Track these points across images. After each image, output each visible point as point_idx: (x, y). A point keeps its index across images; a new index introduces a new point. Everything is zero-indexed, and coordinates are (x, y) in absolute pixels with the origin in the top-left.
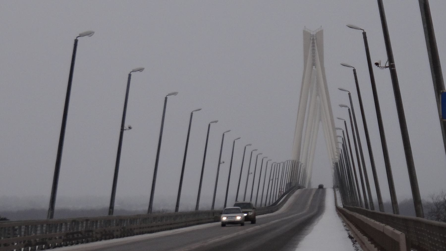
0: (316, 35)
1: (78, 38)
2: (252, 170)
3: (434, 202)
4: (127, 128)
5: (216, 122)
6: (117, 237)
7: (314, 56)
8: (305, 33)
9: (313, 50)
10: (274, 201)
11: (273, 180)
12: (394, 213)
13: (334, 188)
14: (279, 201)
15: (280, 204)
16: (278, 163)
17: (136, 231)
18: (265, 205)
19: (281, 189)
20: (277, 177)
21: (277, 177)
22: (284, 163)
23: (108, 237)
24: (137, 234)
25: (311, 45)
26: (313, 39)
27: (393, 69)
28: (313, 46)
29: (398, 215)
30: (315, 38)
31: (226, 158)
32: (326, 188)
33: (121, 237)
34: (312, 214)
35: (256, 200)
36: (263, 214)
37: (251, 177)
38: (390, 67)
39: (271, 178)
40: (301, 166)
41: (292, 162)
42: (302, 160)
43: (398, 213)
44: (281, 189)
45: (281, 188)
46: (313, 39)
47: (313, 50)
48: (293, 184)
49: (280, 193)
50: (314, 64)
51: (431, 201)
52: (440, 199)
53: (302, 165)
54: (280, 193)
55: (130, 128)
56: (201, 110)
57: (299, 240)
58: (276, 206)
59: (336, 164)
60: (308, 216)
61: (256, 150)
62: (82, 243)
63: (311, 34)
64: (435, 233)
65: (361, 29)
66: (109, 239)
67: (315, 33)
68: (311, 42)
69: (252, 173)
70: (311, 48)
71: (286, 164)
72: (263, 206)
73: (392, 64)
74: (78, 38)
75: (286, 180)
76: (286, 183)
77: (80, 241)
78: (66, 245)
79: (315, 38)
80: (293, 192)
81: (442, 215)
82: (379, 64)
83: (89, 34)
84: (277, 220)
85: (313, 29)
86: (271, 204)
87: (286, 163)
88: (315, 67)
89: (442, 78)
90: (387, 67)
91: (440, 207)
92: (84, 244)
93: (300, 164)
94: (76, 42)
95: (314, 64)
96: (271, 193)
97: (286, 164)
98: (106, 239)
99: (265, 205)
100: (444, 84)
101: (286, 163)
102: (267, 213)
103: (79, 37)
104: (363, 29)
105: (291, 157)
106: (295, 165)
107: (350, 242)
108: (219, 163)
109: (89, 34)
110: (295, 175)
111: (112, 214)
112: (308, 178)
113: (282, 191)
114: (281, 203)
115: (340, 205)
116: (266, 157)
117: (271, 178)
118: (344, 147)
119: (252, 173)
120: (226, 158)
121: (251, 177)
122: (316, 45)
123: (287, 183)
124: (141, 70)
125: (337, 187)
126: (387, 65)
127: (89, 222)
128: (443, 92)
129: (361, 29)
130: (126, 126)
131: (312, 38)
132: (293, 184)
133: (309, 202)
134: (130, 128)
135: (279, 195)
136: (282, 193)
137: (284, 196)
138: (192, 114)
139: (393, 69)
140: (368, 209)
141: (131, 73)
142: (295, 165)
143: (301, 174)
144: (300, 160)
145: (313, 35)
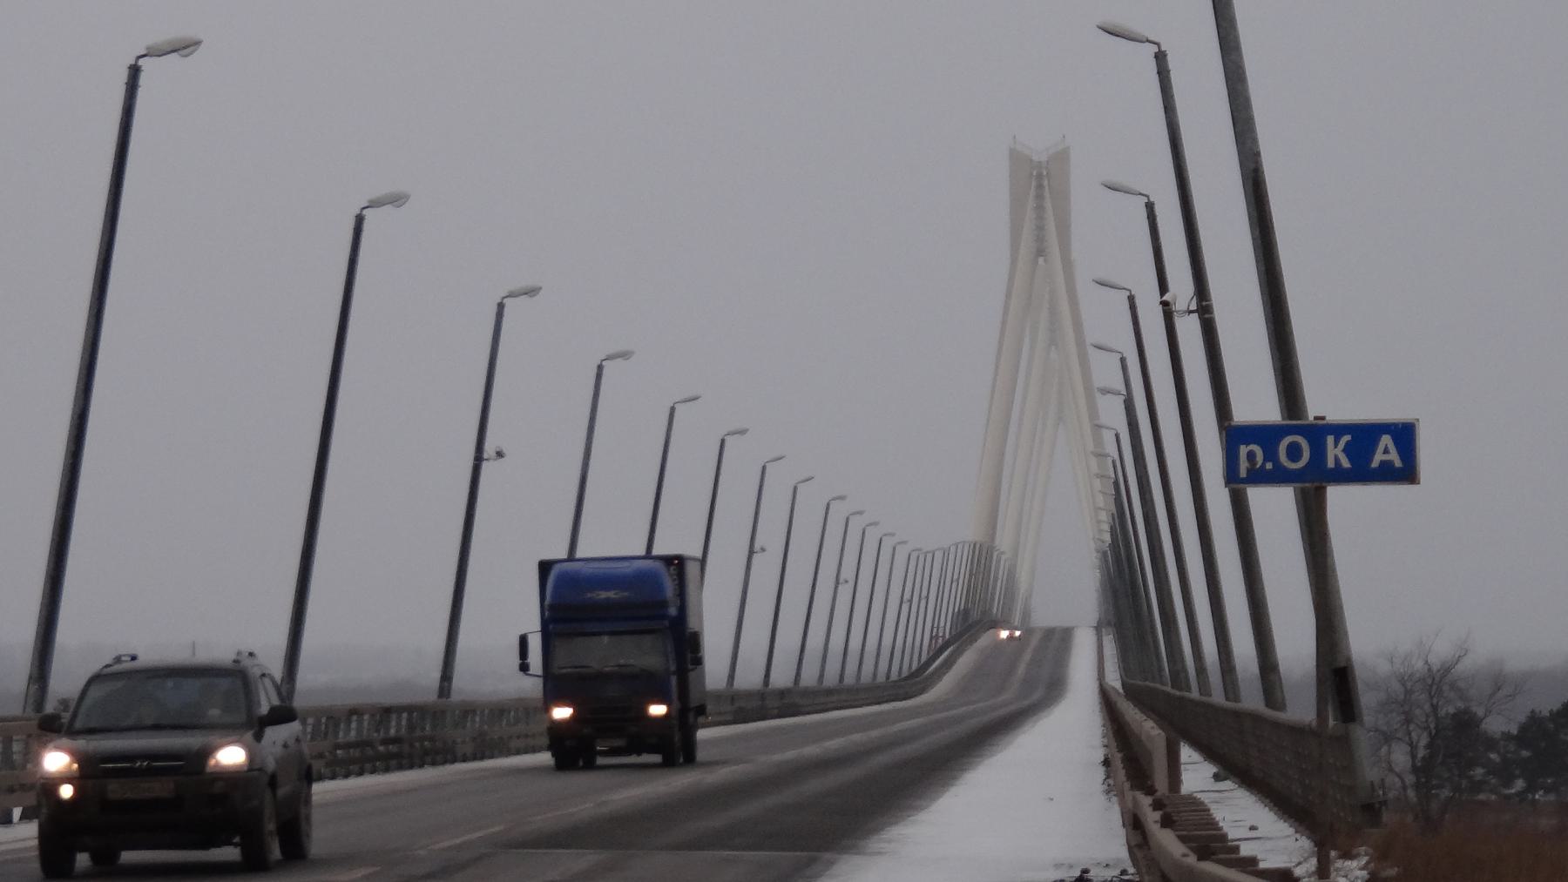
0: (1048, 162)
1: (365, 212)
2: (848, 573)
3: (1429, 670)
4: (493, 454)
5: (742, 432)
6: (465, 759)
7: (1040, 228)
8: (1017, 159)
9: (1040, 208)
10: (915, 666)
11: (911, 601)
12: (1227, 699)
13: (1098, 629)
14: (931, 665)
15: (933, 674)
16: (928, 552)
17: (514, 744)
18: (888, 677)
19: (935, 630)
20: (924, 593)
21: (924, 593)
22: (946, 553)
23: (429, 759)
24: (518, 752)
25: (1033, 192)
26: (1040, 176)
27: (1206, 316)
28: (1039, 197)
29: (1239, 704)
30: (1045, 173)
31: (771, 536)
32: (1073, 628)
33: (474, 758)
34: (1026, 703)
35: (876, 663)
36: (879, 703)
37: (845, 593)
38: (1200, 310)
39: (907, 596)
40: (998, 561)
41: (972, 547)
42: (1004, 541)
43: (1237, 699)
44: (935, 630)
45: (936, 625)
46: (1040, 176)
47: (1040, 208)
48: (975, 615)
49: (934, 642)
50: (1040, 252)
51: (1384, 668)
52: (1413, 662)
53: (1003, 557)
54: (934, 642)
55: (500, 454)
56: (699, 400)
57: (963, 770)
58: (922, 677)
59: (1104, 554)
60: (1012, 708)
61: (860, 513)
62: (373, 772)
63: (1031, 160)
64: (1549, 781)
65: (1140, 194)
66: (444, 762)
67: (1044, 158)
68: (1034, 184)
69: (847, 582)
70: (1031, 203)
71: (952, 557)
72: (881, 678)
73: (1204, 303)
74: (365, 212)
75: (954, 601)
76: (953, 614)
77: (368, 766)
78: (333, 777)
79: (1045, 173)
80: (973, 639)
81: (1418, 712)
82: (1172, 302)
83: (397, 200)
84: (919, 720)
85: (1039, 145)
86: (905, 673)
87: (953, 549)
88: (1045, 261)
89: (1297, 363)
90: (1191, 312)
91: (1412, 686)
92: (379, 774)
93: (995, 554)
94: (359, 221)
95: (1040, 252)
96: (922, 640)
97: (952, 557)
98: (434, 764)
99: (875, 675)
100: (1300, 377)
101: (953, 549)
102: (893, 701)
103: (366, 210)
104: (1145, 193)
105: (968, 531)
106: (982, 558)
107: (1100, 773)
108: (751, 552)
109: (397, 200)
110: (978, 591)
111: (448, 696)
112: (1021, 596)
113: (941, 634)
114: (937, 669)
115: (1114, 680)
116: (892, 535)
117: (907, 596)
118: (1122, 508)
119: (847, 582)
120: (771, 536)
121: (845, 593)
122: (1047, 194)
123: (956, 610)
124: (533, 291)
125: (1109, 624)
126: (1193, 307)
127: (366, 717)
128: (1230, 425)
129: (1140, 194)
130: (489, 449)
131: (1035, 173)
132: (975, 615)
133: (1021, 669)
134: (500, 454)
135: (930, 645)
136: (940, 640)
137: (946, 650)
138: (672, 410)
139: (1206, 316)
140: (1189, 689)
141: (505, 301)
142: (982, 558)
143: (999, 584)
144: (997, 542)
145: (1040, 162)
